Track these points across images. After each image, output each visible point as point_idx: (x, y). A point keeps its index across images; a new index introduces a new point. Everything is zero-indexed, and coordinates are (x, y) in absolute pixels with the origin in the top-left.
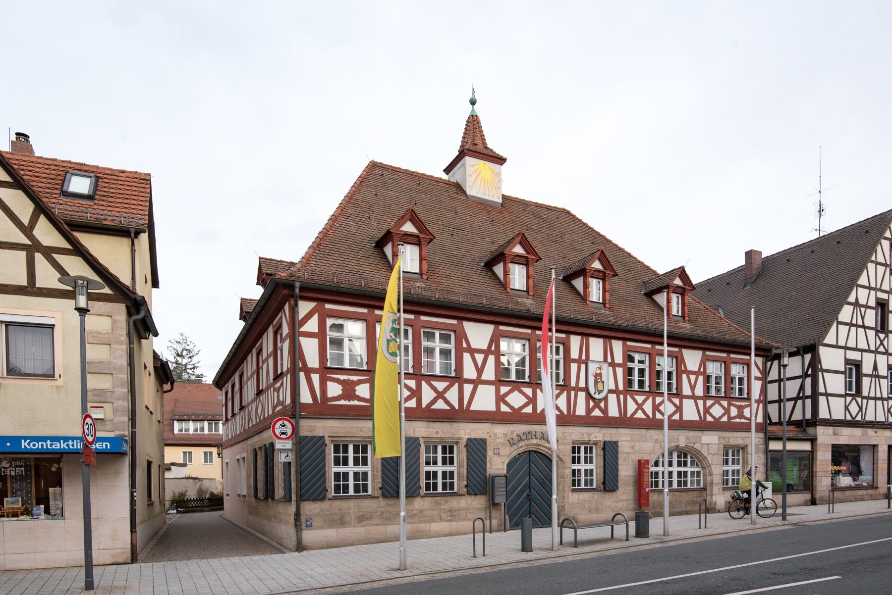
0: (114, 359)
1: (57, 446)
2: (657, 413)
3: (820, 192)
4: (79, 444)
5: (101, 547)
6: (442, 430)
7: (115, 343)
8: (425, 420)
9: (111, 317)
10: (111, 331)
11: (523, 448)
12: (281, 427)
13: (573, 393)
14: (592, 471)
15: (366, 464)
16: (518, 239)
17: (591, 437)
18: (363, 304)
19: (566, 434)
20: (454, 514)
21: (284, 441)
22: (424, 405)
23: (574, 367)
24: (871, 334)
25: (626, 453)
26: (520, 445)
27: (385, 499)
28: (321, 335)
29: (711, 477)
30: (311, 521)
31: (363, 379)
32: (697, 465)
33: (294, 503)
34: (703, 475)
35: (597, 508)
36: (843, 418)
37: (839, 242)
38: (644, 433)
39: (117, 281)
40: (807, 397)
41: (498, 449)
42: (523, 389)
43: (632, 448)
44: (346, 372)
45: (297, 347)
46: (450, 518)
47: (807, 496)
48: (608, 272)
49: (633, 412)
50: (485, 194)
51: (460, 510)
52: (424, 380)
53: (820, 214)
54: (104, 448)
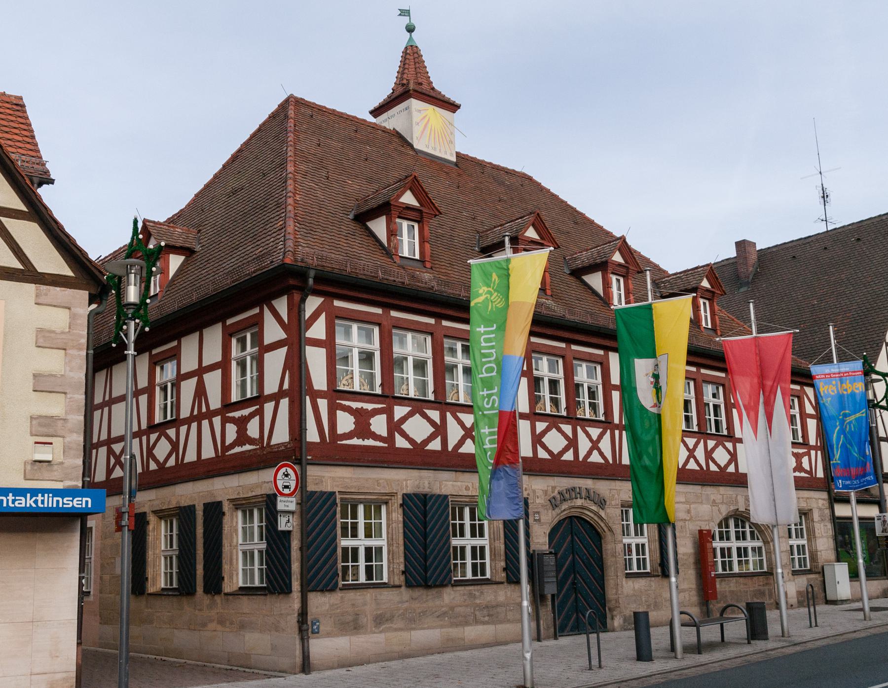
0: (70, 371)
1: (21, 504)
3: (820, 173)
4: (50, 499)
5: (37, 670)
7: (73, 347)
8: (451, 469)
9: (69, 309)
10: (67, 330)
11: (565, 512)
12: (283, 476)
13: (617, 432)
14: (482, 549)
16: (531, 218)
18: (404, 306)
19: (614, 492)
20: (491, 613)
21: (286, 499)
25: (682, 520)
26: (563, 507)
27: (408, 589)
28: (329, 344)
30: (318, 624)
31: (378, 408)
32: (758, 539)
34: (766, 553)
35: (656, 602)
37: (858, 239)
38: (700, 491)
39: (86, 258)
41: (538, 513)
42: (427, 411)
43: (689, 513)
44: (359, 397)
45: (303, 361)
46: (487, 619)
48: (631, 267)
50: (435, 149)
51: (497, 606)
53: (825, 201)
54: (84, 506)
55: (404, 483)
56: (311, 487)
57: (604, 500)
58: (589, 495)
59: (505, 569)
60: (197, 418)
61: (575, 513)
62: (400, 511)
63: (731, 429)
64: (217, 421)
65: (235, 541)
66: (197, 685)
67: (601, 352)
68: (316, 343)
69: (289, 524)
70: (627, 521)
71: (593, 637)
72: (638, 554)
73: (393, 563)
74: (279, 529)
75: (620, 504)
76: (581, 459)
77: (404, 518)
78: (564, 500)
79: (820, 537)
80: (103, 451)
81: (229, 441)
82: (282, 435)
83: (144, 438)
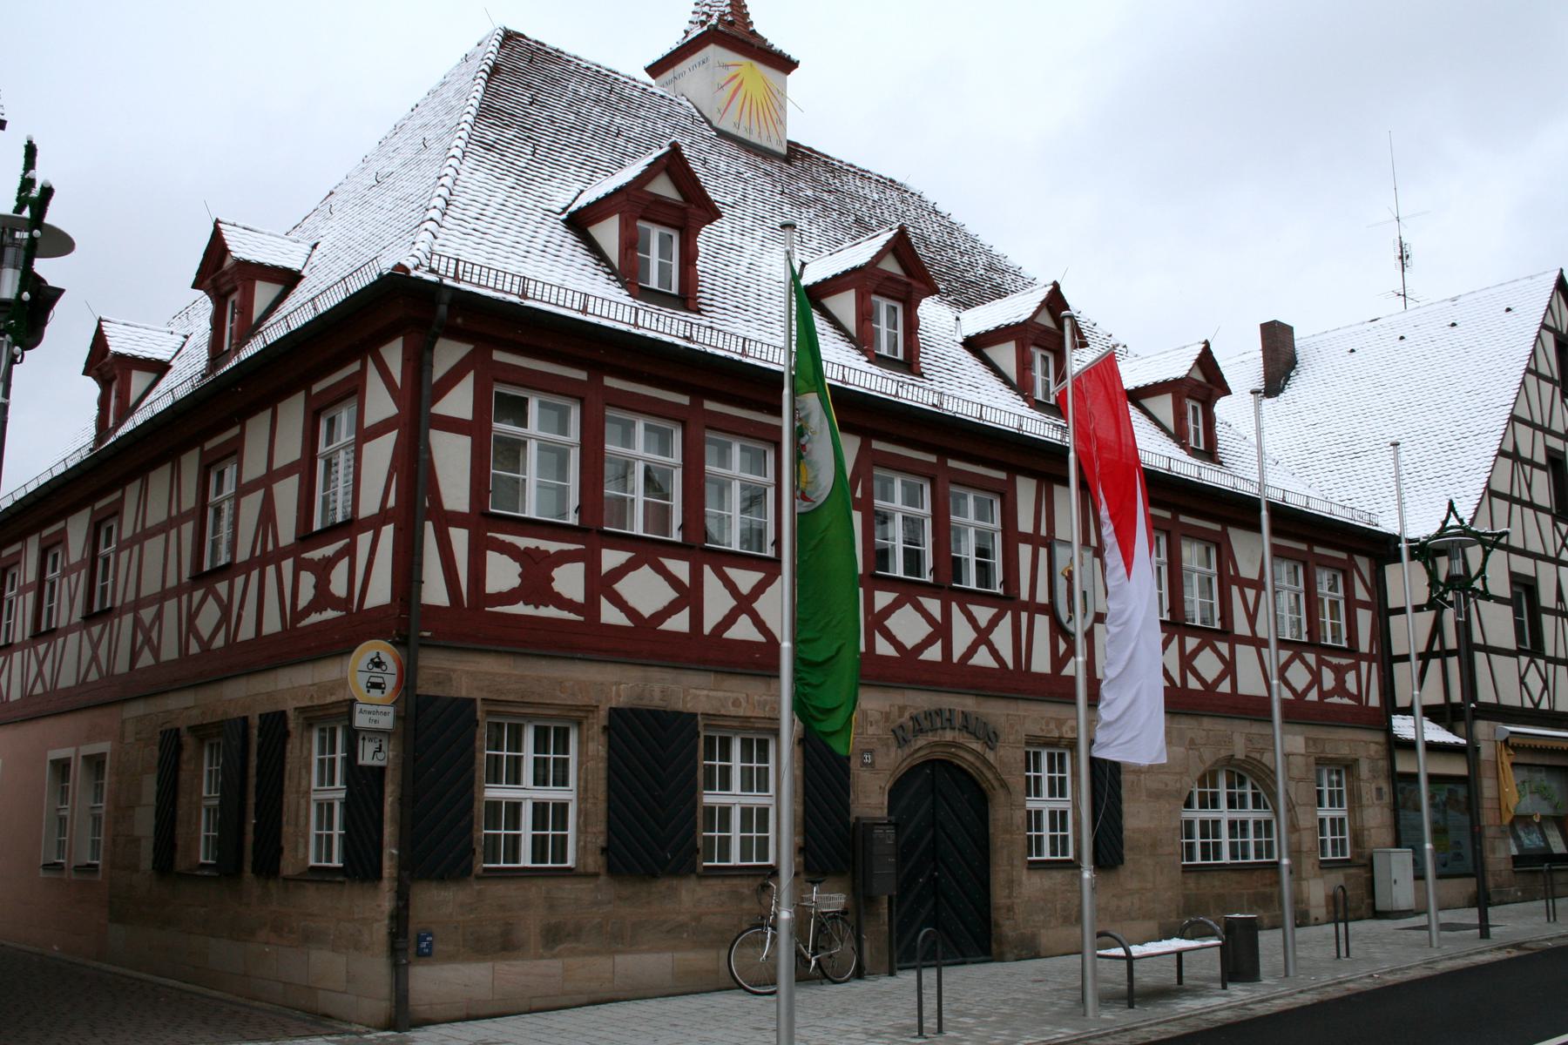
2: (878, 637)
6: (747, 695)
12: (370, 666)
13: (1024, 616)
15: (565, 783)
17: (1065, 729)
22: (707, 628)
23: (1025, 551)
24: (1546, 520)
28: (476, 429)
29: (1297, 834)
31: (569, 551)
32: (1266, 807)
33: (387, 885)
36: (1518, 704)
40: (1451, 653)
47: (1470, 885)
49: (719, 618)
52: (707, 564)
55: (614, 688)
56: (426, 688)
57: (994, 733)
58: (969, 724)
59: (604, 850)
60: (260, 561)
61: (939, 754)
62: (603, 739)
63: (1227, 620)
64: (287, 565)
65: (304, 783)
66: (289, 1035)
67: (1002, 475)
68: (452, 425)
69: (380, 755)
70: (1036, 770)
71: (930, 975)
72: (1053, 828)
73: (586, 832)
74: (360, 762)
75: (1024, 741)
76: (955, 659)
77: (608, 753)
78: (921, 731)
79: (1368, 806)
80: (128, 619)
81: (303, 602)
82: (380, 592)
83: (185, 598)
